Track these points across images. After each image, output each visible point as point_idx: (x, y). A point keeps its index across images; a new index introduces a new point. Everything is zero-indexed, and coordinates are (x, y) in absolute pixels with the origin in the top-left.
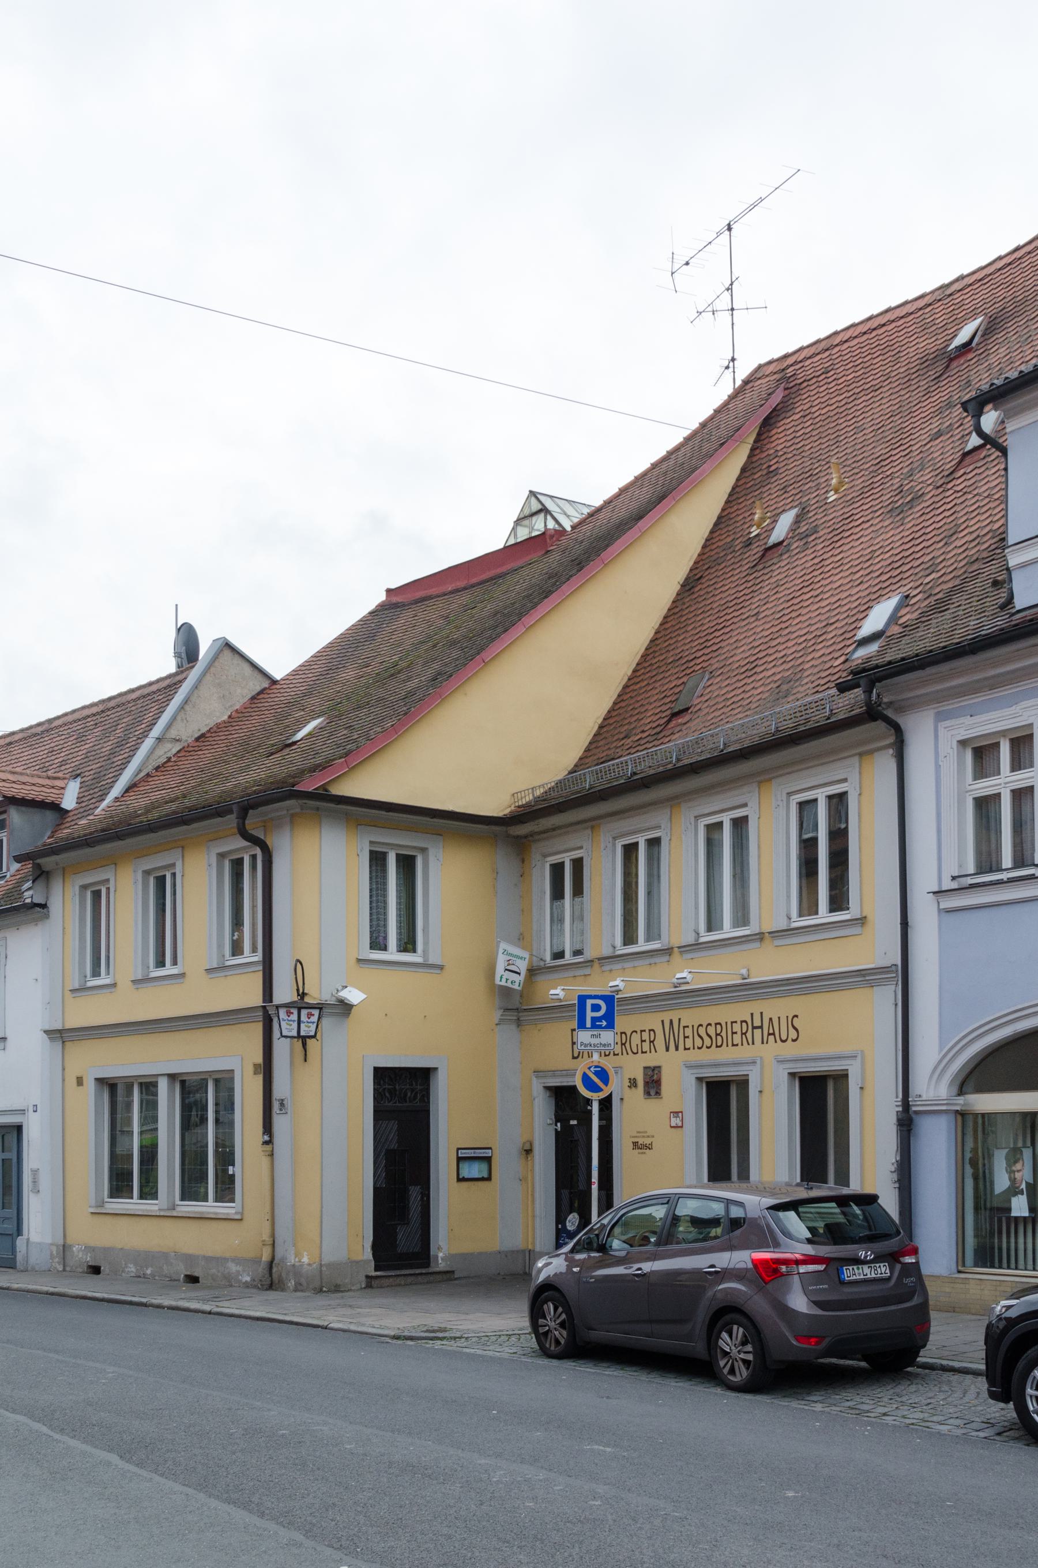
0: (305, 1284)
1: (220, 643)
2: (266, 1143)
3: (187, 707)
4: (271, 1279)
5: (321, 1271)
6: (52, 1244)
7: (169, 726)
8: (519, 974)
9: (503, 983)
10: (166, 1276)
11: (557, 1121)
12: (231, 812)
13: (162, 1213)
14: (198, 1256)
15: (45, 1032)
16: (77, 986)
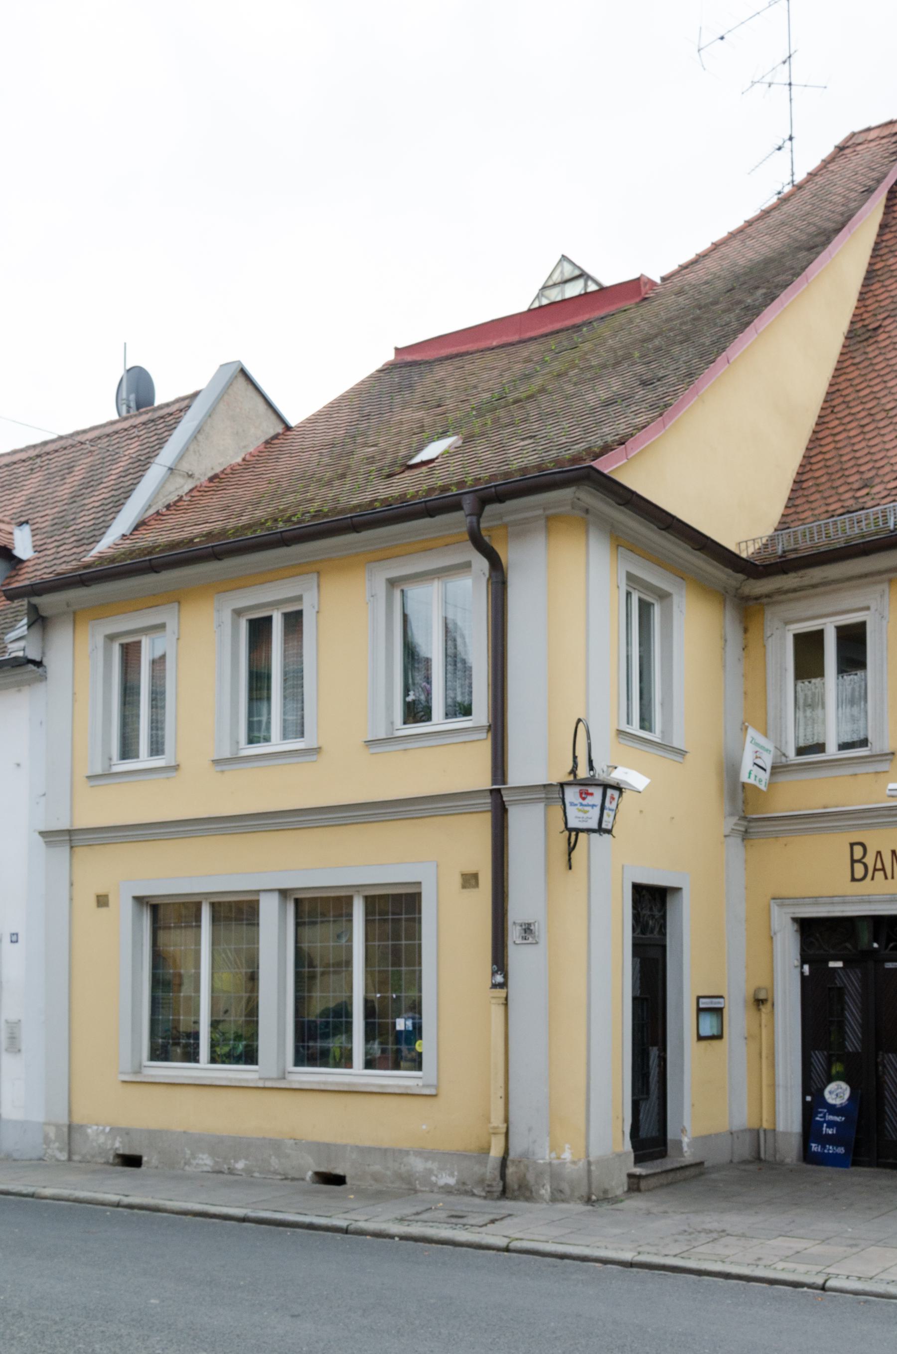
0: (567, 1190)
1: (234, 369)
2: (495, 986)
3: (200, 437)
4: (508, 1184)
5: (589, 1172)
6: (46, 1124)
7: (181, 457)
8: (765, 770)
9: (751, 781)
10: (276, 1173)
11: (803, 962)
12: (456, 506)
13: (269, 1084)
14: (345, 1146)
15: (42, 833)
16: (99, 771)
